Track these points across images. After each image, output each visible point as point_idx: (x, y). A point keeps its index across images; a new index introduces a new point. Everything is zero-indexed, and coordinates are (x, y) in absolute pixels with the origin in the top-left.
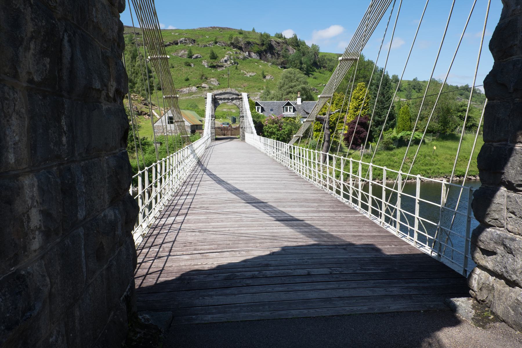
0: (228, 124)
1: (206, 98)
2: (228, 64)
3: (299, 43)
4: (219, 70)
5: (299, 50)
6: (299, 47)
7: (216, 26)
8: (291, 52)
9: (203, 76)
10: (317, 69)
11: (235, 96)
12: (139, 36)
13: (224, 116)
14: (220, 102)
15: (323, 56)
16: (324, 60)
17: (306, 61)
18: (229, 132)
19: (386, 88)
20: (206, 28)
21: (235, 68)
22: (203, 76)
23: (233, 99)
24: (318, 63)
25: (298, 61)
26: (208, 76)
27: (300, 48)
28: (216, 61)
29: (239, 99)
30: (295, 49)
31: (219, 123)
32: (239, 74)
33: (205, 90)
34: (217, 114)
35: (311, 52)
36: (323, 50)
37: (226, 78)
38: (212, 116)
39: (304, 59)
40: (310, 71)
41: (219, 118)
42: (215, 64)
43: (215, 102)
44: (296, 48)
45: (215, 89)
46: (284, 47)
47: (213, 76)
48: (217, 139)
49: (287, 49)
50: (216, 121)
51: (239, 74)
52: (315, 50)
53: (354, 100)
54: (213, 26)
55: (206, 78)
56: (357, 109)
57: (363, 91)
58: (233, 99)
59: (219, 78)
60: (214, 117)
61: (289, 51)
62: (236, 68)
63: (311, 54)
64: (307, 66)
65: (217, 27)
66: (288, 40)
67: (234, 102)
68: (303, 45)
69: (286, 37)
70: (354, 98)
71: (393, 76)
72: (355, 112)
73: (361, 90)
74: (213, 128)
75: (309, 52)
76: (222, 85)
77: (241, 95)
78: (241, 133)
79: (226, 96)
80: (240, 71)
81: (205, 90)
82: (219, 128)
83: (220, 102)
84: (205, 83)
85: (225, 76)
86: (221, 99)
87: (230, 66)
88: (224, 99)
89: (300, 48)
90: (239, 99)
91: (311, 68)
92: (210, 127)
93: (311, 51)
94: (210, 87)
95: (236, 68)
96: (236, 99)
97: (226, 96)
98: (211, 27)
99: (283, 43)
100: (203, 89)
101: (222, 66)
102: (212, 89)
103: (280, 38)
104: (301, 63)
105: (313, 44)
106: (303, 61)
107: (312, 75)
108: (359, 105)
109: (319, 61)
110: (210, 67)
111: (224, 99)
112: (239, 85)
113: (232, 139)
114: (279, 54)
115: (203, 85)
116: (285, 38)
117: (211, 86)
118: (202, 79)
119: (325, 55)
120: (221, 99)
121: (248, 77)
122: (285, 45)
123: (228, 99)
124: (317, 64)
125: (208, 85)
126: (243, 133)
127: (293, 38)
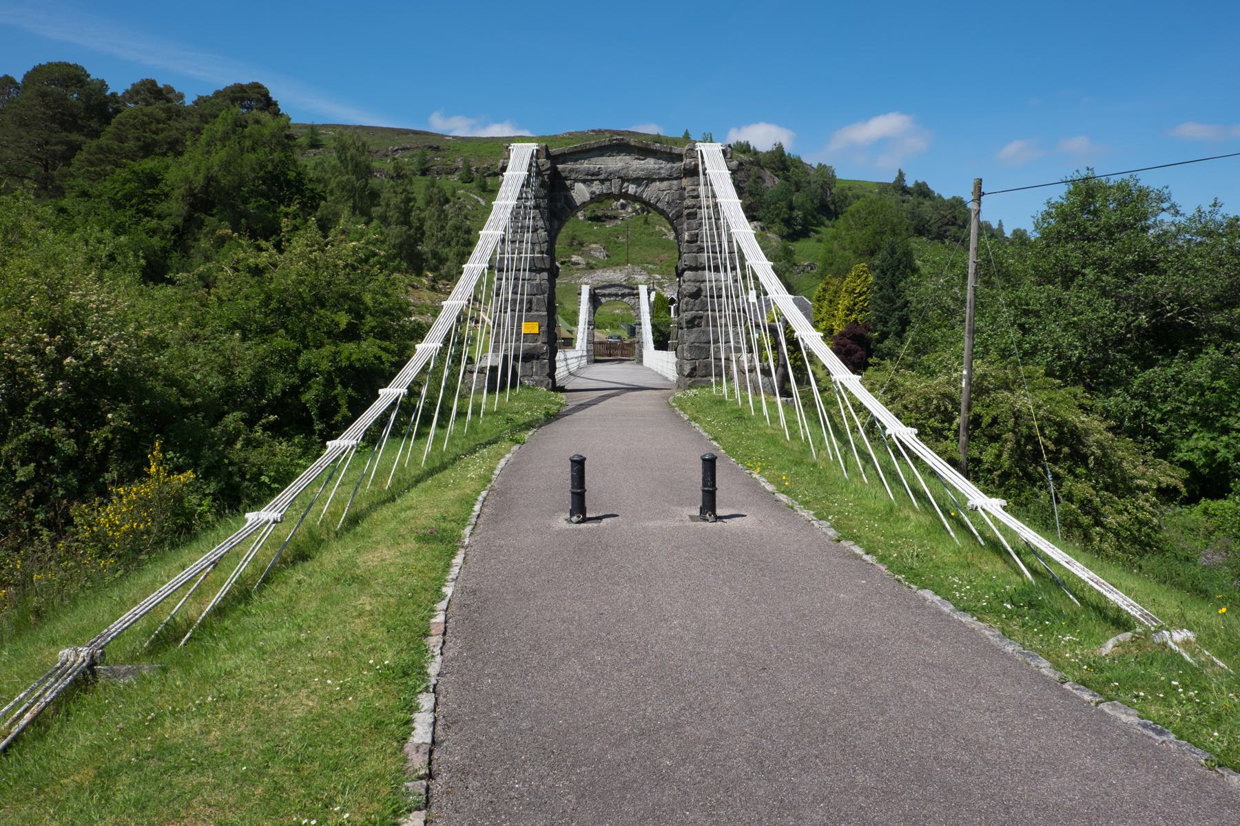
0: (619, 338)
1: (580, 294)
2: (627, 213)
3: (789, 163)
4: (609, 225)
5: (787, 179)
6: (788, 171)
7: (603, 127)
8: (768, 183)
9: (573, 239)
10: (828, 218)
11: (627, 291)
12: (439, 153)
13: (615, 323)
14: (603, 300)
15: (842, 190)
16: (846, 198)
17: (802, 204)
18: (619, 352)
19: (897, 274)
20: (583, 133)
21: (643, 220)
22: (573, 239)
23: (623, 296)
24: (832, 207)
25: (783, 203)
26: (585, 239)
27: (790, 173)
28: (602, 206)
29: (634, 295)
30: (778, 176)
31: (601, 335)
32: (651, 235)
33: (578, 269)
34: (599, 319)
35: (815, 182)
36: (845, 173)
37: (623, 243)
38: (590, 323)
39: (797, 198)
40: (813, 225)
41: (605, 328)
42: (600, 213)
43: (595, 299)
44: (781, 173)
45: (599, 268)
46: (752, 172)
47: (596, 239)
48: (596, 361)
49: (759, 177)
50: (597, 333)
51: (651, 235)
52: (826, 176)
53: (846, 295)
54: (596, 128)
55: (581, 244)
56: (850, 310)
57: (863, 278)
58: (623, 296)
59: (609, 244)
60: (593, 324)
61: (764, 181)
62: (646, 222)
63: (813, 186)
64: (805, 216)
65: (606, 131)
66: (761, 157)
67: (626, 300)
68: (796, 167)
69: (759, 149)
70: (846, 291)
71: (1015, 232)
72: (847, 316)
73: (859, 277)
74: (591, 341)
75: (809, 183)
76: (614, 259)
77: (637, 288)
78: (637, 351)
79: (613, 290)
80: (654, 227)
81: (578, 269)
82: (601, 343)
83: (603, 300)
84: (579, 255)
85: (622, 239)
86: (604, 295)
87: (632, 217)
88: (610, 295)
89: (790, 173)
90: (634, 295)
91: (814, 217)
92: (585, 341)
93: (815, 179)
94: (588, 264)
95: (646, 222)
96: (629, 295)
97: (613, 290)
98: (593, 131)
99: (752, 163)
100: (574, 267)
101: (615, 218)
102: (592, 268)
103: (744, 152)
104: (791, 208)
105: (820, 164)
106: (795, 204)
107: (817, 232)
108: (855, 304)
109: (834, 203)
110: (590, 219)
111: (610, 295)
112: (650, 259)
113: (621, 361)
114: (742, 188)
115: (575, 258)
116: (756, 153)
117: (590, 261)
118: (571, 245)
119: (851, 185)
120: (604, 295)
121: (669, 241)
122: (756, 168)
123: (616, 295)
124: (828, 207)
125: (585, 258)
126: (641, 352)
127: (772, 152)
